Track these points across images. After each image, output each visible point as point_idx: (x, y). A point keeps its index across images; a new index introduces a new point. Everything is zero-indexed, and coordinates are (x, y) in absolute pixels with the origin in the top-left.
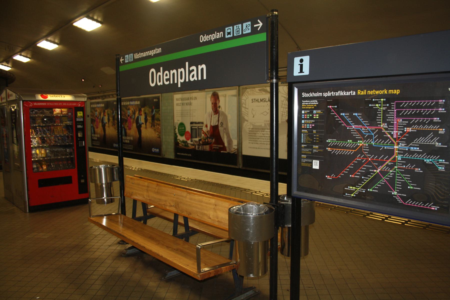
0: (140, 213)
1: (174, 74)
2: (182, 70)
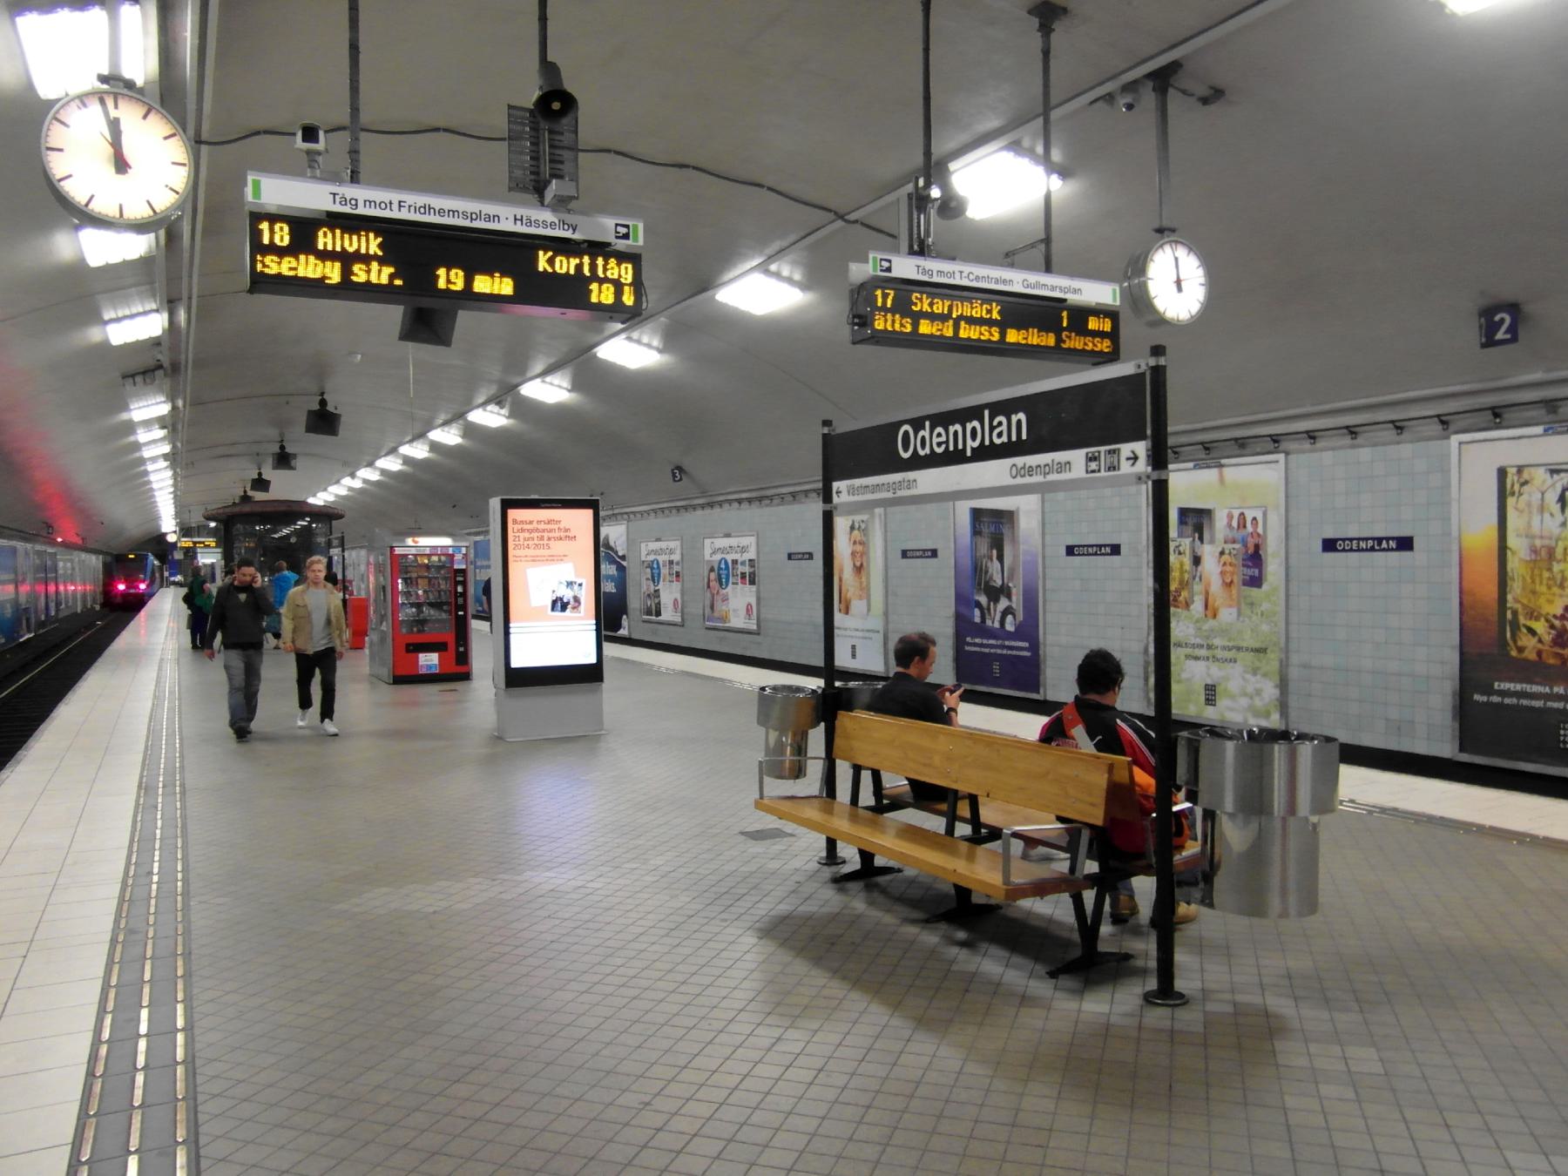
0: (867, 798)
1: (956, 433)
2: (976, 423)
